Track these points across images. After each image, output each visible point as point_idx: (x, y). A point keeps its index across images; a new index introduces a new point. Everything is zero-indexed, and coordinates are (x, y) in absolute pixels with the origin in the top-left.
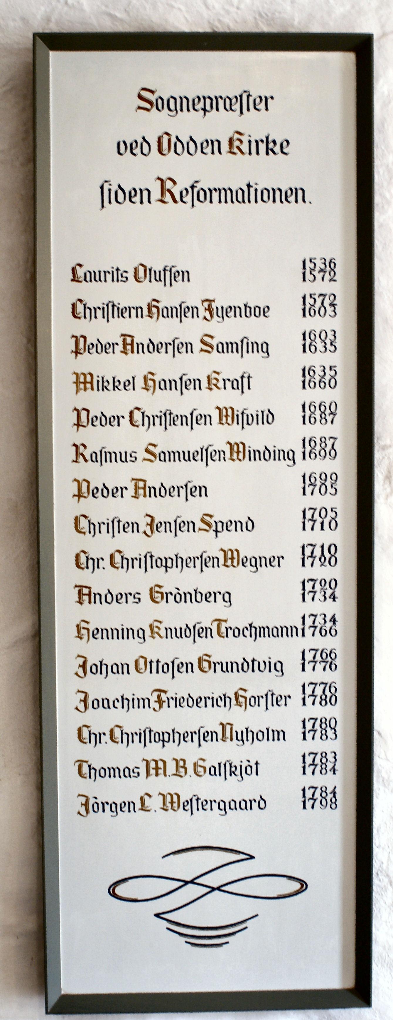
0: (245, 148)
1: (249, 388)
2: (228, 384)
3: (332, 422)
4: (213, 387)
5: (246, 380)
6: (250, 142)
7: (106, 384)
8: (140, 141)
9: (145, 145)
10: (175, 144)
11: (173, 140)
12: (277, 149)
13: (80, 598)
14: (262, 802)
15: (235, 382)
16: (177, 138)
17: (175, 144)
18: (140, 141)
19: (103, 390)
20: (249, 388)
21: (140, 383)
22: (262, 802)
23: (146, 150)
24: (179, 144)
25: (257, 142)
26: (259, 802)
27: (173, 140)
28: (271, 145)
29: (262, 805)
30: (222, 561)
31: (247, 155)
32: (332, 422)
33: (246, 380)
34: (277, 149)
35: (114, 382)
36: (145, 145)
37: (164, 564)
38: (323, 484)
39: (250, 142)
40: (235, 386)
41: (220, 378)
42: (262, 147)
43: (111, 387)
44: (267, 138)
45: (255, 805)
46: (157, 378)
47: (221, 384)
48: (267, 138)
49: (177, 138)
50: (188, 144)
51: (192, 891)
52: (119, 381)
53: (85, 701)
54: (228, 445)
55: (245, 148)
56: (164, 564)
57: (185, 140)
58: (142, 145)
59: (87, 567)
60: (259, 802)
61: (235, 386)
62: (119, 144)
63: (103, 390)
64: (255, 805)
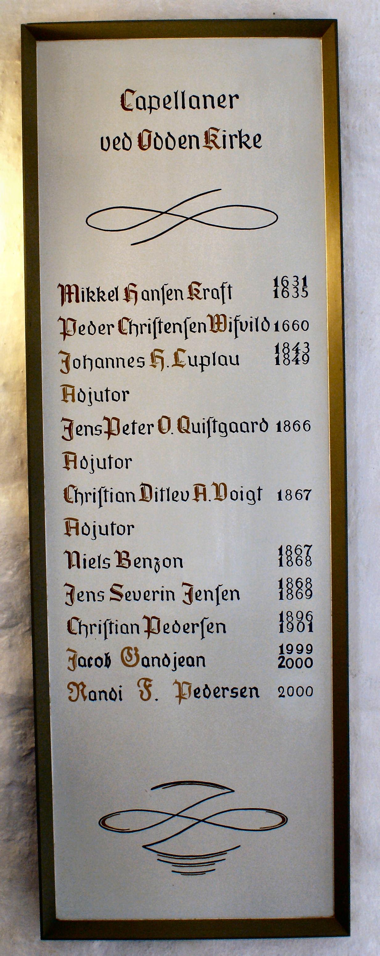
0: (220, 142)
1: (230, 298)
2: (208, 294)
3: (307, 499)
4: (194, 297)
5: (226, 290)
6: (224, 137)
7: (91, 295)
8: (122, 137)
9: (126, 140)
10: (155, 140)
11: (153, 136)
12: (250, 143)
13: (68, 530)
14: (264, 424)
15: (215, 292)
16: (157, 134)
17: (155, 140)
18: (122, 137)
19: (88, 301)
20: (230, 298)
21: (122, 294)
22: (264, 424)
23: (127, 146)
24: (158, 140)
25: (231, 137)
26: (261, 424)
27: (153, 136)
28: (244, 139)
29: (264, 426)
30: (208, 327)
31: (222, 148)
32: (307, 499)
33: (226, 290)
34: (250, 143)
35: (99, 293)
36: (126, 140)
37: (147, 105)
38: (300, 588)
39: (224, 137)
40: (215, 296)
41: (201, 288)
42: (236, 141)
43: (95, 297)
44: (240, 132)
45: (257, 427)
46: (139, 289)
47: (201, 295)
48: (240, 132)
49: (157, 134)
50: (167, 139)
51: (179, 824)
52: (103, 292)
53: (67, 362)
54: (209, 318)
55: (220, 142)
56: (147, 105)
57: (164, 136)
58: (123, 140)
59: (76, 501)
60: (261, 424)
61: (215, 296)
62: (102, 139)
63: (88, 301)
64: (257, 427)
